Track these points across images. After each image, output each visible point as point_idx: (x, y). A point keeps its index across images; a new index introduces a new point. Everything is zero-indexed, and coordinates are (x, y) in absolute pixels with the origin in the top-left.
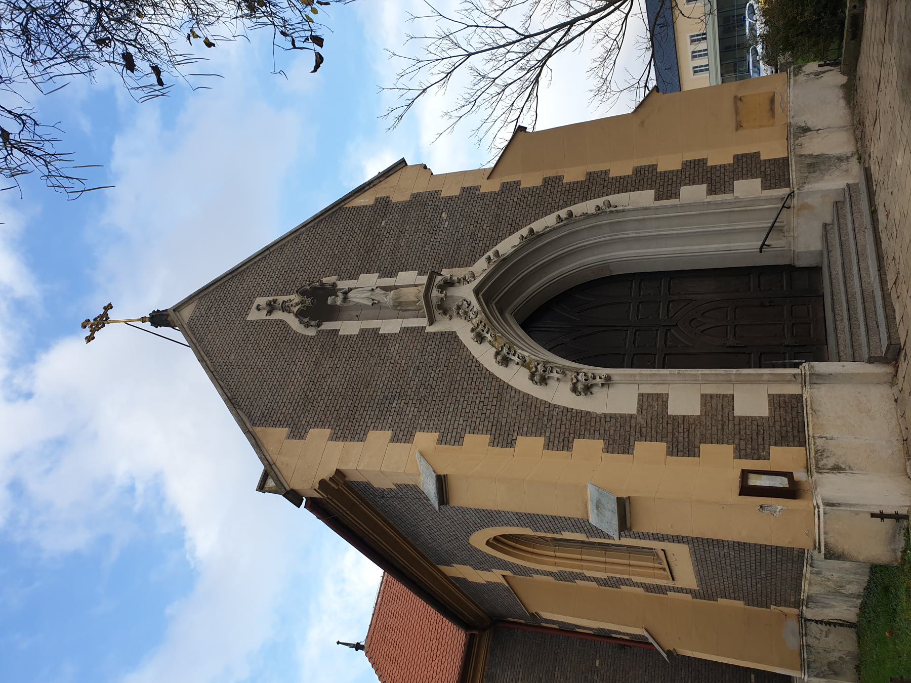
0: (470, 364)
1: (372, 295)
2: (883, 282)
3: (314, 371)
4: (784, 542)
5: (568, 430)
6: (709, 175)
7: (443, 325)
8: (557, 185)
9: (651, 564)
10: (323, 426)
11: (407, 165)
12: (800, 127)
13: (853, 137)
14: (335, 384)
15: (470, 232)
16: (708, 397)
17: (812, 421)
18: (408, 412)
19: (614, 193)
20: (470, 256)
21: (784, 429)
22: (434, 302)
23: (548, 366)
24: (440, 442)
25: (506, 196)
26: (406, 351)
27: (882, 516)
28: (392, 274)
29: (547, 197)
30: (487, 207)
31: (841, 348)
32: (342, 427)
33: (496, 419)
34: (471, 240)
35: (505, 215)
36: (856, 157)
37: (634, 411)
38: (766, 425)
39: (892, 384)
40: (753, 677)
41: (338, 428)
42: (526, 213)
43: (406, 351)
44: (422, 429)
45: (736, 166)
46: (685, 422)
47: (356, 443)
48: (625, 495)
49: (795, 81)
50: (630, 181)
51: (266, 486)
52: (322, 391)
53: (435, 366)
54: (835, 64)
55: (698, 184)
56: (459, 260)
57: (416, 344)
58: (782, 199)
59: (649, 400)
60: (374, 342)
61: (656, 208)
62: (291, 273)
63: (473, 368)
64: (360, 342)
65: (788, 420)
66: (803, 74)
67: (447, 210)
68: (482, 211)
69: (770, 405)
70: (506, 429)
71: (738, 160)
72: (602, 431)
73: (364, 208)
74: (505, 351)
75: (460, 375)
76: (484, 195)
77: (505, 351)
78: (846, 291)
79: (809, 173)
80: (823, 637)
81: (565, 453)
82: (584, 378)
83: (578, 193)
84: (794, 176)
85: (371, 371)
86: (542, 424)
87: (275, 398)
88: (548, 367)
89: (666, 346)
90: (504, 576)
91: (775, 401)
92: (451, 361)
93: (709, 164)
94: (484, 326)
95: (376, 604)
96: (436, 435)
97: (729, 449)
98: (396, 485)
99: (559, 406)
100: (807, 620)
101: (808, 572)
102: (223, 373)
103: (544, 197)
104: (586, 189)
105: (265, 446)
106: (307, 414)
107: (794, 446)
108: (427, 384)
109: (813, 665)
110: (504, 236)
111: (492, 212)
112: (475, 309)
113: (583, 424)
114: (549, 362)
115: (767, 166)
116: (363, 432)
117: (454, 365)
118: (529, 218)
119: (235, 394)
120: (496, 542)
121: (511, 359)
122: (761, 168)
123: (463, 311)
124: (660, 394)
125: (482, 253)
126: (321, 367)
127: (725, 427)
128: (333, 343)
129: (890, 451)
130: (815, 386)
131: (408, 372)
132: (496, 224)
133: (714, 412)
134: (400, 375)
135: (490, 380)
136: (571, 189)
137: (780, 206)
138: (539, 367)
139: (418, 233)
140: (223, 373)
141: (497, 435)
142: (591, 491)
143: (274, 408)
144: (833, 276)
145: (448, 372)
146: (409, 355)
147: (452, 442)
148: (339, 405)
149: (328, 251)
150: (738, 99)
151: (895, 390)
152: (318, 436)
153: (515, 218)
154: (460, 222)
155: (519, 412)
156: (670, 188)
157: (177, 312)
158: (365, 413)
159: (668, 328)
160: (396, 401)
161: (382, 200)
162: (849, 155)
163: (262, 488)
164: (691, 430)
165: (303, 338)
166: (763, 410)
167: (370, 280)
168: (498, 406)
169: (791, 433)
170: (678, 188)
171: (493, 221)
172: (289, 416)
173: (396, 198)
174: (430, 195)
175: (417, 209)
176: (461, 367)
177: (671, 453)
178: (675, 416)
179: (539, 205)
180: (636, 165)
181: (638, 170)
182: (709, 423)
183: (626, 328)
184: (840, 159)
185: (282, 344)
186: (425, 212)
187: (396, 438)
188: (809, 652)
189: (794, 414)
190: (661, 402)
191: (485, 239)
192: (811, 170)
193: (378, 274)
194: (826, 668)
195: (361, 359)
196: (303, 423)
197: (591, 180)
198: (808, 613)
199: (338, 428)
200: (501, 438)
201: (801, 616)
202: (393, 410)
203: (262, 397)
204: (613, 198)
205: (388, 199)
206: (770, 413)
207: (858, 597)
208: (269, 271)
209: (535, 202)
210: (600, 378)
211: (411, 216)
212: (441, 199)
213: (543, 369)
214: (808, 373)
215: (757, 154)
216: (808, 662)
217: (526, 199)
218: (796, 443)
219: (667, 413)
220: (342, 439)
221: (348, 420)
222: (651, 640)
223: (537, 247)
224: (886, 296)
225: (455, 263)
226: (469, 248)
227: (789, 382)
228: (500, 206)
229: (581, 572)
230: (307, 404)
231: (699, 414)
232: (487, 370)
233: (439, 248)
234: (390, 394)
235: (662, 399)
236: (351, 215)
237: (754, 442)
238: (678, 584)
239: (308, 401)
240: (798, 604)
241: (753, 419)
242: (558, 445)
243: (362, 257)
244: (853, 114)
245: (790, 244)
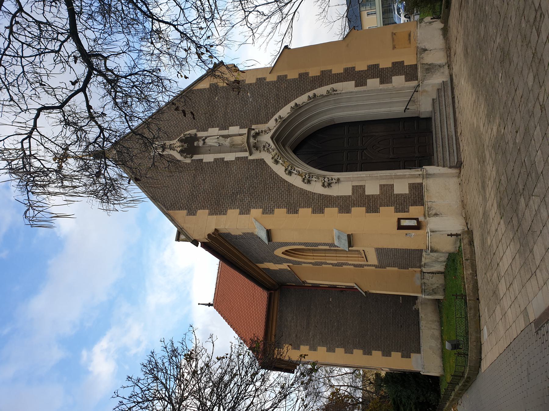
0: (273, 175)
1: (218, 140)
2: (456, 132)
4: (415, 247)
5: (322, 204)
6: (380, 73)
7: (256, 156)
8: (306, 78)
9: (357, 256)
10: (204, 209)
12: (422, 49)
13: (446, 54)
17: (427, 195)
18: (245, 200)
19: (335, 83)
20: (266, 118)
21: (415, 198)
22: (252, 144)
23: (311, 175)
24: (263, 213)
27: (451, 235)
28: (226, 128)
29: (302, 84)
31: (439, 160)
32: (214, 208)
34: (265, 109)
35: (281, 95)
36: (447, 65)
37: (351, 194)
39: (459, 177)
40: (401, 298)
42: (292, 93)
44: (254, 208)
48: (350, 233)
49: (420, 26)
51: (180, 239)
54: (438, 18)
56: (260, 120)
58: (415, 87)
62: (170, 128)
63: (274, 177)
65: (417, 194)
66: (424, 22)
69: (409, 188)
72: (337, 204)
74: (290, 168)
75: (268, 181)
76: (269, 83)
77: (290, 168)
78: (442, 134)
79: (426, 73)
80: (431, 279)
82: (327, 180)
83: (317, 83)
84: (419, 74)
85: (224, 180)
88: (311, 175)
89: (362, 159)
90: (288, 266)
93: (380, 67)
94: (278, 156)
95: (217, 283)
96: (261, 210)
97: (392, 209)
98: (244, 233)
100: (424, 273)
101: (425, 254)
104: (321, 80)
109: (426, 291)
110: (282, 106)
111: (274, 93)
112: (272, 147)
114: (311, 173)
120: (286, 253)
123: (266, 148)
125: (272, 116)
126: (197, 179)
129: (456, 206)
130: (428, 179)
133: (385, 193)
134: (238, 182)
136: (313, 80)
137: (414, 90)
138: (306, 175)
139: (236, 105)
141: (289, 209)
142: (335, 232)
144: (436, 125)
145: (263, 179)
147: (269, 213)
150: (394, 34)
151: (459, 180)
152: (203, 214)
153: (286, 96)
154: (258, 99)
155: (299, 197)
158: (224, 201)
159: (363, 150)
160: (239, 195)
162: (444, 64)
163: (178, 239)
166: (406, 191)
167: (214, 131)
171: (275, 98)
172: (185, 204)
177: (367, 212)
178: (368, 195)
179: (298, 89)
181: (346, 70)
182: (383, 198)
183: (343, 151)
184: (440, 66)
187: (242, 212)
188: (425, 286)
189: (419, 192)
192: (427, 72)
194: (431, 291)
195: (217, 174)
197: (323, 75)
198: (424, 270)
199: (212, 209)
201: (421, 271)
202: (238, 199)
203: (169, 196)
204: (335, 86)
206: (409, 192)
207: (445, 262)
210: (335, 180)
212: (246, 85)
213: (308, 176)
214: (425, 173)
216: (424, 290)
217: (291, 85)
218: (420, 205)
220: (215, 214)
221: (216, 205)
222: (357, 287)
223: (298, 113)
224: (457, 139)
225: (258, 122)
226: (265, 113)
227: (417, 177)
228: (278, 90)
229: (325, 261)
230: (193, 198)
232: (281, 178)
233: (249, 113)
234: (235, 192)
235: (363, 188)
238: (369, 263)
240: (420, 267)
241: (402, 195)
242: (318, 211)
244: (446, 43)
245: (418, 108)
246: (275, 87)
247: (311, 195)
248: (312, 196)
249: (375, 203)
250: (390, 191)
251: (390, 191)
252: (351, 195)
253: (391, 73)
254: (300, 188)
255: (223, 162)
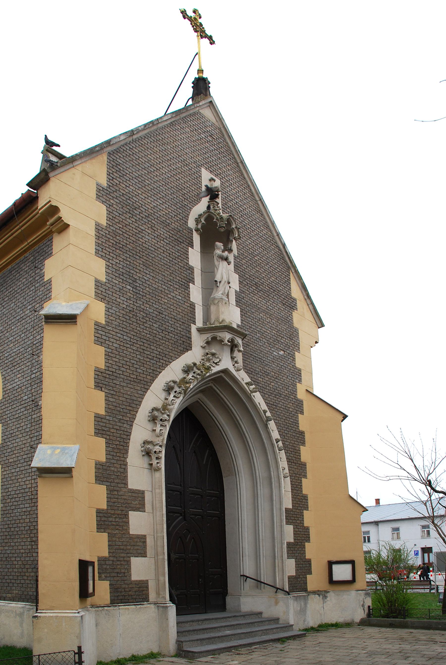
3: (157, 219)
6: (299, 544)
8: (299, 441)
10: (108, 219)
11: (319, 328)
14: (146, 237)
15: (269, 372)
16: (144, 540)
19: (291, 481)
21: (123, 590)
25: (293, 402)
26: (175, 305)
29: (291, 433)
30: (287, 387)
33: (118, 376)
34: (263, 372)
37: (130, 487)
38: (125, 578)
41: (107, 232)
42: (281, 417)
43: (175, 305)
44: (107, 309)
45: (304, 560)
46: (124, 523)
47: (94, 247)
50: (299, 492)
52: (140, 224)
53: (163, 328)
55: (294, 537)
56: (249, 360)
57: (181, 314)
59: (140, 498)
60: (183, 277)
61: (280, 509)
64: (182, 265)
65: (130, 593)
67: (285, 355)
68: (284, 383)
69: (140, 581)
70: (110, 384)
71: (308, 561)
72: (113, 461)
73: (289, 288)
75: (155, 349)
76: (295, 386)
81: (92, 431)
83: (292, 455)
85: (158, 271)
86: (116, 414)
87: (134, 179)
91: (143, 585)
92: (167, 343)
97: (105, 553)
99: (132, 429)
102: (155, 134)
103: (292, 431)
105: (90, 161)
106: (120, 206)
107: (110, 596)
108: (147, 319)
110: (265, 398)
113: (118, 446)
115: (303, 579)
116: (104, 254)
117: (164, 345)
118: (278, 418)
119: (137, 142)
121: (170, 394)
122: (302, 575)
124: (145, 506)
126: (161, 226)
127: (122, 551)
128: (182, 241)
131: (157, 303)
132: (274, 393)
133: (132, 544)
135: (151, 374)
139: (269, 329)
140: (155, 134)
141: (105, 375)
143: (125, 176)
144: (228, 619)
146: (172, 307)
148: (128, 237)
149: (257, 251)
153: (278, 408)
156: (292, 518)
157: (208, 105)
160: (131, 289)
161: (294, 303)
164: (118, 527)
165: (186, 215)
166: (135, 576)
168: (129, 378)
169: (120, 595)
170: (292, 524)
172: (117, 188)
173: (296, 316)
174: (297, 343)
175: (288, 331)
176: (162, 351)
177: (99, 512)
180: (309, 496)
181: (305, 498)
182: (124, 539)
185: (181, 195)
186: (285, 337)
187: (99, 284)
190: (139, 507)
191: (263, 383)
193: (238, 290)
196: (112, 201)
197: (301, 466)
199: (107, 232)
200: (103, 378)
202: (124, 285)
205: (295, 309)
206: (134, 581)
208: (242, 197)
209: (288, 424)
210: (158, 463)
211: (282, 326)
212: (294, 352)
215: (310, 573)
217: (290, 417)
218: (113, 598)
219: (130, 511)
225: (246, 357)
228: (286, 397)
230: (128, 207)
231: (131, 533)
232: (160, 372)
233: (258, 345)
234: (138, 285)
235: (141, 508)
236: (284, 276)
237: (111, 570)
239: (131, 209)
241: (129, 569)
242: (99, 425)
243: (252, 279)
246: (290, 393)
247: (128, 419)
248: (127, 421)
249: (113, 525)
250: (135, 552)
251: (135, 552)
252: (129, 487)
253: (298, 557)
254: (141, 402)
255: (188, 280)
